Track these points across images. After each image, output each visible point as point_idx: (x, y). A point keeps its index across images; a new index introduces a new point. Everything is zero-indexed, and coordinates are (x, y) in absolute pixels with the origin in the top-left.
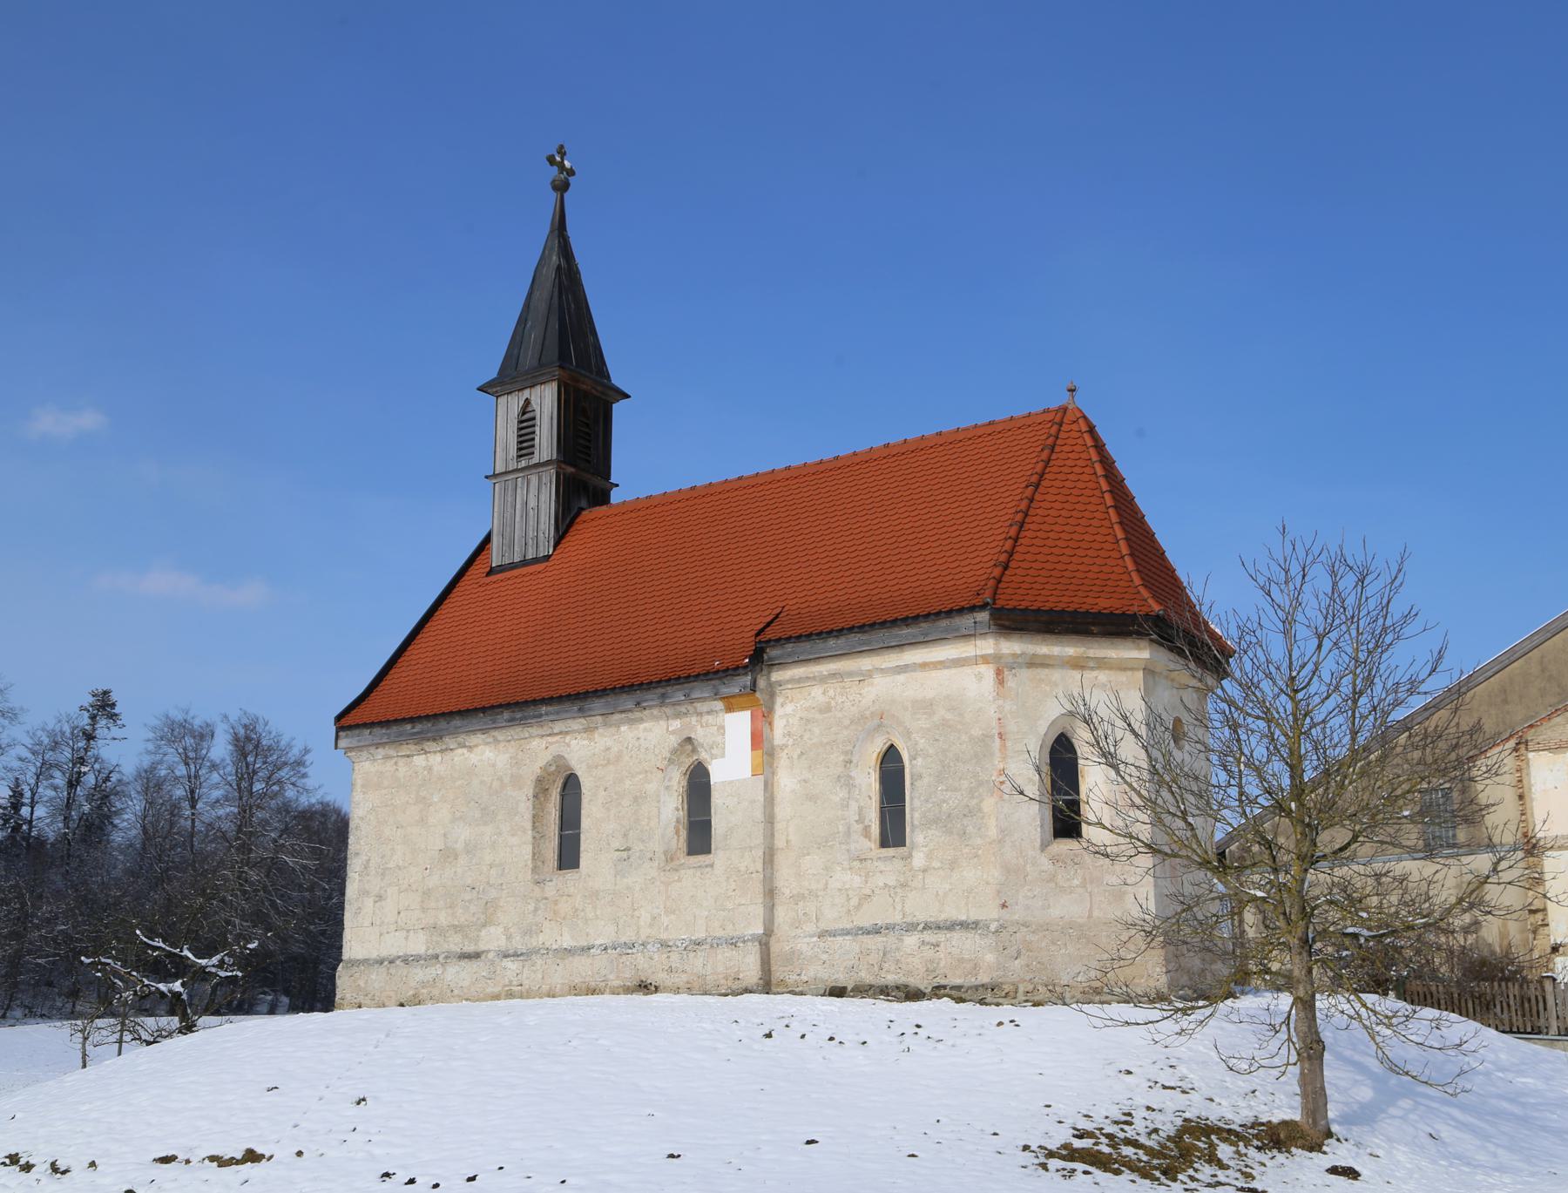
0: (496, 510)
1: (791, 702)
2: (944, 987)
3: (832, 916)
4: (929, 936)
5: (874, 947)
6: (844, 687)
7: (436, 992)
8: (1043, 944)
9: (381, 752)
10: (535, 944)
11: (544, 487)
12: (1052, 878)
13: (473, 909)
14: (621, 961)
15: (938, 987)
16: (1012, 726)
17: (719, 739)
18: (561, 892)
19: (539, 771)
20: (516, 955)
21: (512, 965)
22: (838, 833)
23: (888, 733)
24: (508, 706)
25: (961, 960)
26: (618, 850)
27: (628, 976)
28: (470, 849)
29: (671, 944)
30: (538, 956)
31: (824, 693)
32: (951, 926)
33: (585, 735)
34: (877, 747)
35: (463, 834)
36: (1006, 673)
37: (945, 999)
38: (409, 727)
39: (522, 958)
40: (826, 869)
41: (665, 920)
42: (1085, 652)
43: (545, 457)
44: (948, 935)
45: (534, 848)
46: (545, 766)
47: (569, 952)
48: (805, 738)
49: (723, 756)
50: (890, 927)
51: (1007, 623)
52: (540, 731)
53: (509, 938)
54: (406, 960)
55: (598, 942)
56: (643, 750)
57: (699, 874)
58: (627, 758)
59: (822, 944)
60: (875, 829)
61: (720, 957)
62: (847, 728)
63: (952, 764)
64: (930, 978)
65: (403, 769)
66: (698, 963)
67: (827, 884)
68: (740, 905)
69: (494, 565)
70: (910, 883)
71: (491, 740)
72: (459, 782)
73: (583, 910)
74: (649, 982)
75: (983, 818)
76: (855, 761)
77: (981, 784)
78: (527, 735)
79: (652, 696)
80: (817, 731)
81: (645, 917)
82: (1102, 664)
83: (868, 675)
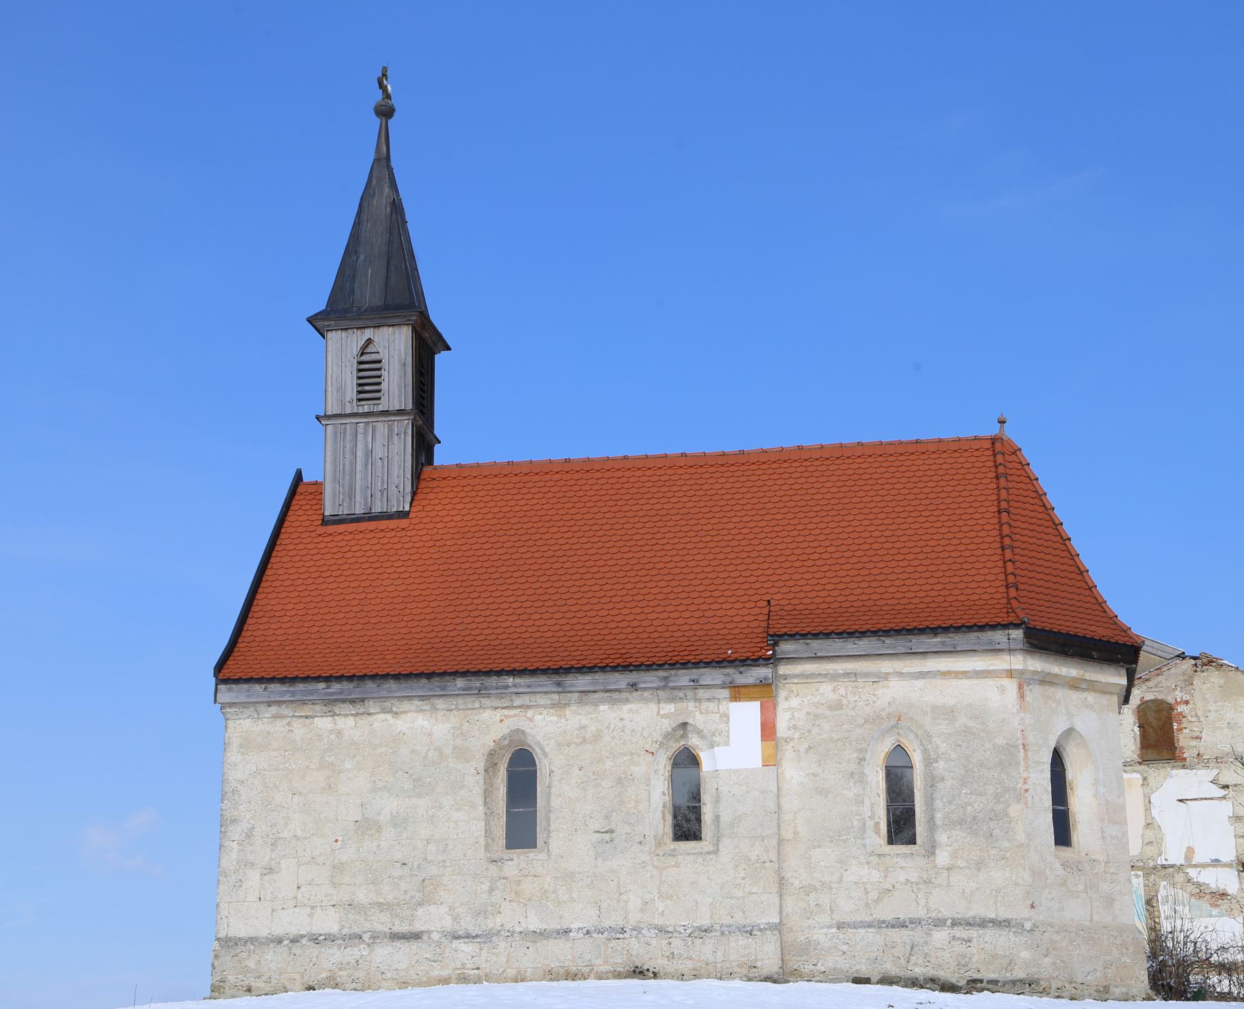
0: (329, 454)
1: (796, 697)
2: (981, 981)
3: (848, 908)
4: (959, 932)
5: (899, 940)
6: (856, 687)
8: (1064, 944)
10: (491, 926)
11: (396, 438)
12: (1064, 884)
13: (403, 886)
14: (611, 945)
15: (975, 981)
16: (1031, 739)
17: (722, 726)
18: (525, 872)
19: (492, 744)
20: (468, 936)
21: (465, 948)
22: (853, 827)
23: (899, 734)
25: (995, 956)
27: (620, 961)
28: (398, 822)
29: (670, 929)
30: (501, 938)
31: (834, 691)
32: (983, 923)
33: (552, 711)
34: (888, 744)
35: (388, 806)
36: (1025, 688)
37: (986, 992)
38: (322, 685)
39: (479, 940)
40: (841, 862)
41: (661, 906)
44: (980, 932)
45: (486, 824)
46: (500, 740)
47: (542, 935)
49: (727, 744)
50: (916, 922)
51: (1035, 642)
52: (496, 703)
53: (456, 918)
54: (315, 939)
55: (575, 926)
57: (700, 860)
58: (607, 738)
59: (841, 936)
61: (733, 944)
62: (860, 726)
63: (975, 769)
64: (962, 972)
65: (299, 730)
66: (706, 950)
67: (841, 877)
68: (750, 893)
69: (327, 513)
70: (933, 880)
72: (383, 750)
73: (554, 892)
74: (645, 967)
75: (1010, 822)
76: (868, 760)
77: (1007, 790)
79: (650, 679)
80: (826, 726)
81: (634, 902)
83: (886, 676)
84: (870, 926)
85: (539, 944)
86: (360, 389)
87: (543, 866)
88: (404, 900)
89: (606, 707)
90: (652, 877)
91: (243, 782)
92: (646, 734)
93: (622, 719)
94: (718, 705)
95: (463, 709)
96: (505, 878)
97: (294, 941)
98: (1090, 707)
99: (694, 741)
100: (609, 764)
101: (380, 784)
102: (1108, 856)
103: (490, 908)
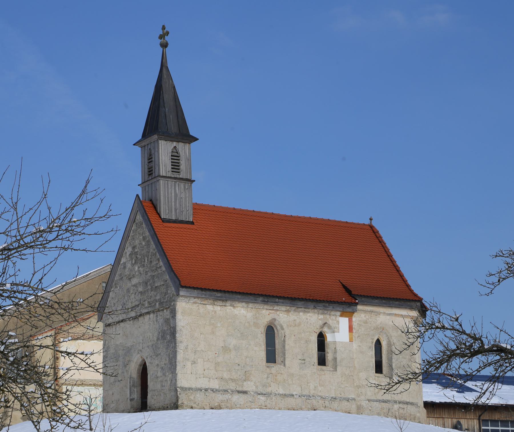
4: (401, 405)
6: (371, 316)
7: (229, 405)
9: (193, 300)
10: (268, 391)
18: (278, 372)
20: (262, 394)
24: (262, 295)
26: (300, 360)
28: (237, 348)
32: (407, 403)
33: (285, 313)
39: (266, 396)
41: (320, 388)
48: (359, 331)
49: (338, 332)
53: (257, 387)
56: (309, 324)
58: (303, 325)
59: (370, 404)
61: (343, 404)
62: (372, 330)
71: (246, 306)
72: (230, 320)
73: (287, 380)
80: (363, 329)
81: (312, 386)
83: (379, 313)
84: (377, 401)
85: (285, 399)
86: (173, 167)
87: (284, 370)
88: (239, 378)
89: (302, 314)
90: (317, 378)
91: (183, 327)
92: (314, 325)
93: (307, 319)
94: (336, 317)
95: (257, 308)
96: (272, 374)
97: (206, 390)
99: (325, 330)
100: (303, 335)
101: (230, 334)
103: (267, 384)
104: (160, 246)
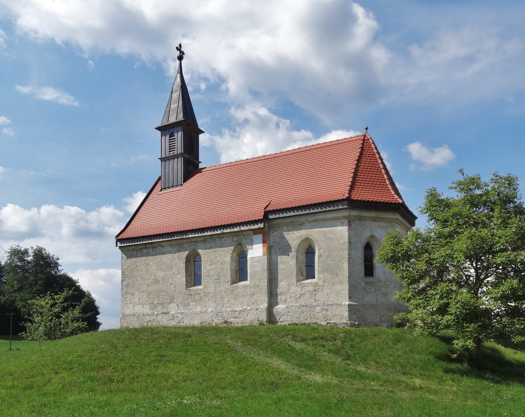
12: (365, 289)
18: (196, 293)
26: (216, 279)
42: (377, 216)
43: (179, 152)
60: (305, 273)
78: (183, 242)
82: (382, 219)
93: (222, 243)
98: (382, 227)
102: (386, 279)
104: (410, 216)
